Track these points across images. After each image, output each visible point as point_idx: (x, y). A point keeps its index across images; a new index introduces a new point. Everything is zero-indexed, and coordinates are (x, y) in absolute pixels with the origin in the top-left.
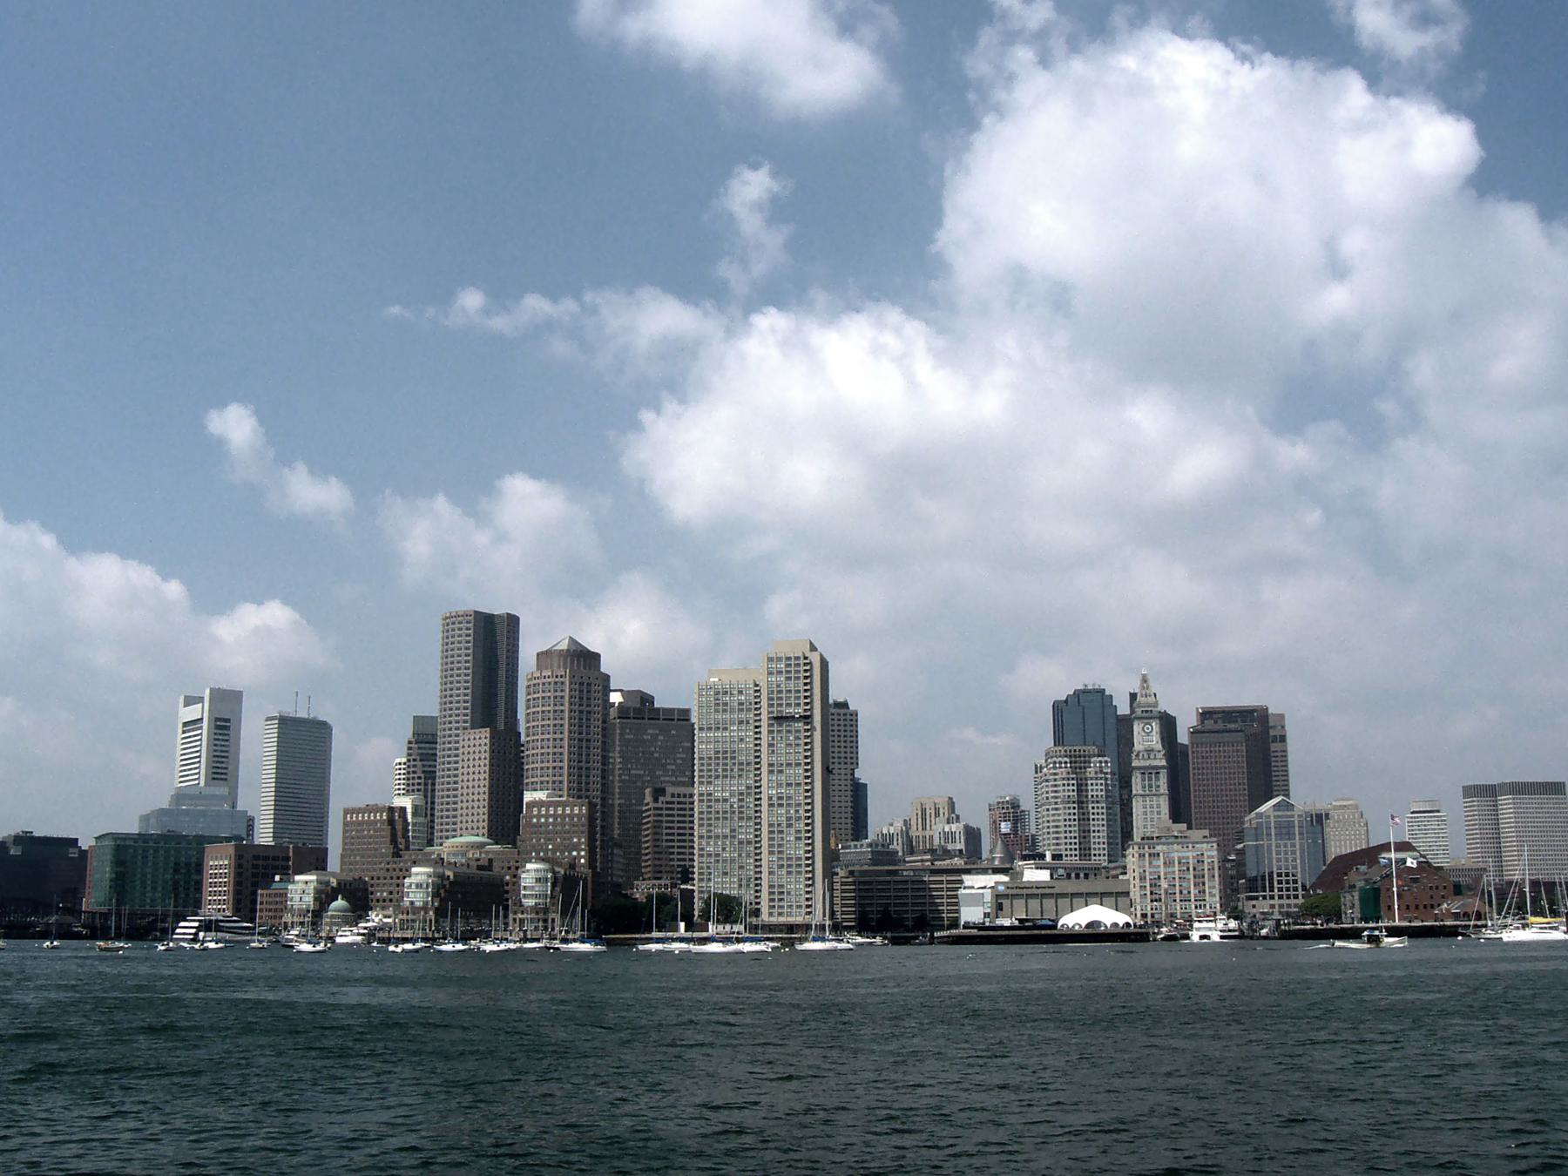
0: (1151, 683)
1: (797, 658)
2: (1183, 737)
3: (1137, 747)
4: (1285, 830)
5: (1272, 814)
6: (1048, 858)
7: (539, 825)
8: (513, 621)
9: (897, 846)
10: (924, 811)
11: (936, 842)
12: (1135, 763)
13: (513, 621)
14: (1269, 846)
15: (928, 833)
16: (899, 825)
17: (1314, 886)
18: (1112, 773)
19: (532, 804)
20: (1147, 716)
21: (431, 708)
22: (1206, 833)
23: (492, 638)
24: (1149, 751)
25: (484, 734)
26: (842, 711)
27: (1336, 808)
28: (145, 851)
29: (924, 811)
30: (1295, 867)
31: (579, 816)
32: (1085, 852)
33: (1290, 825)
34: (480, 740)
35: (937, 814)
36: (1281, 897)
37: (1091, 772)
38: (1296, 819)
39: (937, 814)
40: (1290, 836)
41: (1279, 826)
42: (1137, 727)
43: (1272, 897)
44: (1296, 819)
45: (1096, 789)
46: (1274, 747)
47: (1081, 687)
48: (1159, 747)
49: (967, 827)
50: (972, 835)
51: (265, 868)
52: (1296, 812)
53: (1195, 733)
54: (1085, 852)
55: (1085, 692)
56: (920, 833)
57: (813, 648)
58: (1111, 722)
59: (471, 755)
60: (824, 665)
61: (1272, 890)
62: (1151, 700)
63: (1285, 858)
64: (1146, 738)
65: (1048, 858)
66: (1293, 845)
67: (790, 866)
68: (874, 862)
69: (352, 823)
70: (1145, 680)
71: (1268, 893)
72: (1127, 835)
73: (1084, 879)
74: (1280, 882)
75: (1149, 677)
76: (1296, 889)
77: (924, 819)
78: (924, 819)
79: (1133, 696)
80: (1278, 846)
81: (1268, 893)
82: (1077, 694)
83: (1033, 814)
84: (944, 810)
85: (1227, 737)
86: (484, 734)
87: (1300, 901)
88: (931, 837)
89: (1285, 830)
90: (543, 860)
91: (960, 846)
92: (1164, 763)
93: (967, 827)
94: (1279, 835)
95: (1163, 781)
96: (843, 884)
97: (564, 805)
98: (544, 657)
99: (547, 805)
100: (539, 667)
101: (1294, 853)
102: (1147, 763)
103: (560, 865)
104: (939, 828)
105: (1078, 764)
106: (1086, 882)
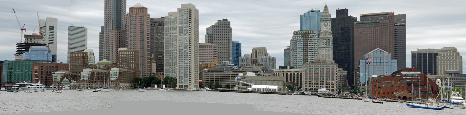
1: (188, 9)
7: (122, 57)
15: (257, 59)
21: (103, 25)
24: (326, 32)
26: (225, 22)
28: (19, 65)
29: (256, 52)
34: (114, 33)
35: (261, 53)
39: (261, 53)
47: (310, 10)
48: (330, 31)
51: (50, 69)
56: (255, 59)
69: (73, 57)
70: (326, 7)
77: (256, 55)
78: (256, 55)
87: (149, 76)
92: (332, 36)
98: (131, 9)
99: (126, 51)
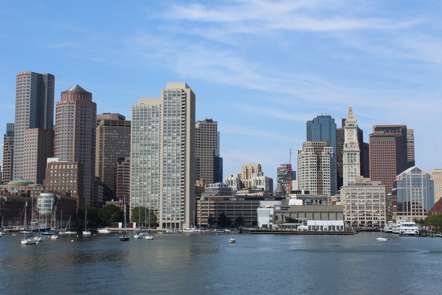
0: (353, 111)
2: (366, 140)
3: (346, 141)
4: (417, 182)
5: (410, 174)
6: (303, 193)
8: (51, 77)
9: (234, 187)
10: (247, 170)
11: (252, 184)
12: (345, 149)
13: (51, 77)
14: (409, 190)
15: (249, 180)
16: (236, 176)
17: (432, 210)
18: (334, 154)
19: (52, 164)
20: (351, 126)
22: (380, 182)
23: (41, 87)
25: (35, 131)
26: (209, 124)
27: (433, 173)
29: (247, 170)
30: (421, 200)
31: (74, 170)
32: (320, 191)
33: (419, 180)
34: (33, 134)
35: (253, 172)
36: (414, 214)
37: (324, 153)
38: (422, 177)
39: (253, 172)
40: (419, 185)
41: (414, 180)
42: (346, 132)
43: (409, 214)
44: (422, 177)
45: (326, 161)
46: (408, 144)
49: (266, 178)
50: (270, 182)
52: (422, 174)
53: (372, 136)
54: (320, 191)
55: (322, 117)
56: (245, 180)
57: (187, 87)
58: (333, 133)
59: (30, 139)
60: (193, 96)
61: (409, 210)
62: (353, 120)
63: (414, 195)
64: (350, 138)
65: (303, 193)
66: (420, 190)
67: (215, 186)
68: (221, 194)
71: (407, 212)
72: (340, 183)
73: (315, 203)
74: (413, 207)
75: (352, 109)
76: (421, 211)
79: (344, 120)
80: (413, 190)
81: (407, 212)
82: (318, 118)
83: (297, 173)
84: (256, 170)
85: (387, 139)
86: (35, 131)
88: (250, 182)
89: (417, 182)
90: (49, 192)
91: (263, 186)
93: (266, 178)
94: (414, 184)
95: (358, 157)
96: (202, 204)
97: (66, 164)
98: (64, 93)
99: (58, 164)
100: (62, 99)
101: (421, 193)
102: (351, 149)
103: (59, 194)
104: (254, 178)
105: (318, 151)
106: (334, 224)
